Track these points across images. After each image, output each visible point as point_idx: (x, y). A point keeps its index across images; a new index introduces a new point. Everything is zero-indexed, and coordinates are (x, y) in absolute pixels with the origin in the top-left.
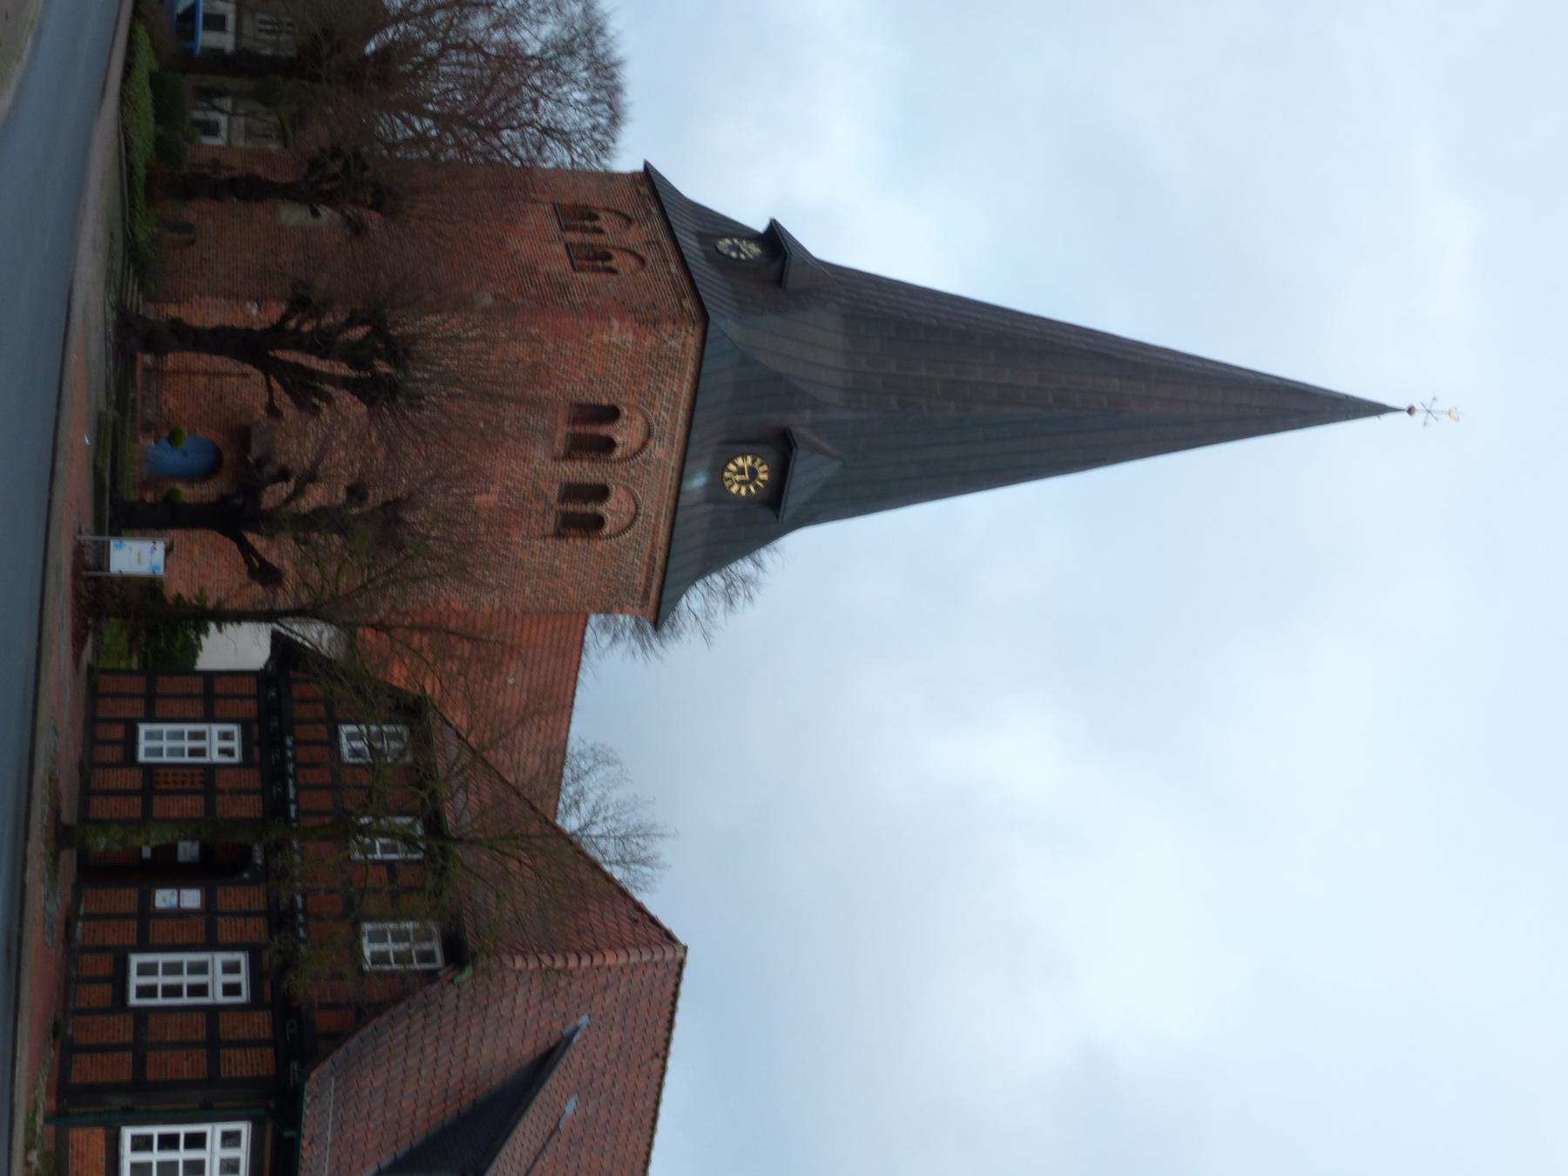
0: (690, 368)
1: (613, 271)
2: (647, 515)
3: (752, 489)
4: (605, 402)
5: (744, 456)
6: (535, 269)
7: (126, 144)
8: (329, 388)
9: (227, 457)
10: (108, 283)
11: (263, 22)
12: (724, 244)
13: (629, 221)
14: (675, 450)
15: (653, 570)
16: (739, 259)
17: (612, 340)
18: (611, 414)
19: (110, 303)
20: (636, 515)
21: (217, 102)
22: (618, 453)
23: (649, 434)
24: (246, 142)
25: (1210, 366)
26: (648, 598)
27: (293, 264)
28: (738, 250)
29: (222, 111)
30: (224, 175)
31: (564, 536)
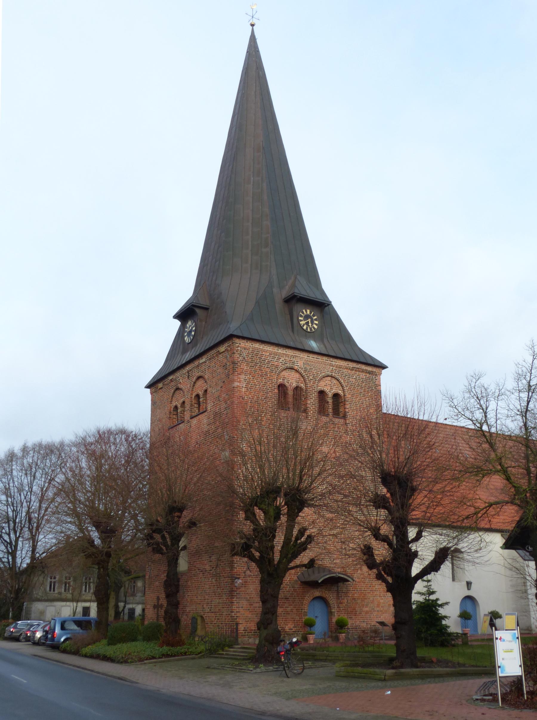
0: (257, 345)
1: (206, 391)
4: (276, 391)
5: (299, 321)
6: (206, 432)
7: (150, 659)
8: (295, 532)
9: (317, 593)
10: (241, 671)
11: (85, 591)
12: (187, 339)
13: (178, 389)
14: (299, 355)
15: (359, 368)
16: (195, 331)
17: (244, 386)
18: (282, 387)
19: (255, 668)
20: (331, 376)
21: (121, 609)
23: (292, 368)
24: (137, 596)
25: (237, 111)
26: (373, 372)
27: (211, 561)
28: (190, 332)
29: (124, 607)
30: (164, 602)
31: (345, 414)
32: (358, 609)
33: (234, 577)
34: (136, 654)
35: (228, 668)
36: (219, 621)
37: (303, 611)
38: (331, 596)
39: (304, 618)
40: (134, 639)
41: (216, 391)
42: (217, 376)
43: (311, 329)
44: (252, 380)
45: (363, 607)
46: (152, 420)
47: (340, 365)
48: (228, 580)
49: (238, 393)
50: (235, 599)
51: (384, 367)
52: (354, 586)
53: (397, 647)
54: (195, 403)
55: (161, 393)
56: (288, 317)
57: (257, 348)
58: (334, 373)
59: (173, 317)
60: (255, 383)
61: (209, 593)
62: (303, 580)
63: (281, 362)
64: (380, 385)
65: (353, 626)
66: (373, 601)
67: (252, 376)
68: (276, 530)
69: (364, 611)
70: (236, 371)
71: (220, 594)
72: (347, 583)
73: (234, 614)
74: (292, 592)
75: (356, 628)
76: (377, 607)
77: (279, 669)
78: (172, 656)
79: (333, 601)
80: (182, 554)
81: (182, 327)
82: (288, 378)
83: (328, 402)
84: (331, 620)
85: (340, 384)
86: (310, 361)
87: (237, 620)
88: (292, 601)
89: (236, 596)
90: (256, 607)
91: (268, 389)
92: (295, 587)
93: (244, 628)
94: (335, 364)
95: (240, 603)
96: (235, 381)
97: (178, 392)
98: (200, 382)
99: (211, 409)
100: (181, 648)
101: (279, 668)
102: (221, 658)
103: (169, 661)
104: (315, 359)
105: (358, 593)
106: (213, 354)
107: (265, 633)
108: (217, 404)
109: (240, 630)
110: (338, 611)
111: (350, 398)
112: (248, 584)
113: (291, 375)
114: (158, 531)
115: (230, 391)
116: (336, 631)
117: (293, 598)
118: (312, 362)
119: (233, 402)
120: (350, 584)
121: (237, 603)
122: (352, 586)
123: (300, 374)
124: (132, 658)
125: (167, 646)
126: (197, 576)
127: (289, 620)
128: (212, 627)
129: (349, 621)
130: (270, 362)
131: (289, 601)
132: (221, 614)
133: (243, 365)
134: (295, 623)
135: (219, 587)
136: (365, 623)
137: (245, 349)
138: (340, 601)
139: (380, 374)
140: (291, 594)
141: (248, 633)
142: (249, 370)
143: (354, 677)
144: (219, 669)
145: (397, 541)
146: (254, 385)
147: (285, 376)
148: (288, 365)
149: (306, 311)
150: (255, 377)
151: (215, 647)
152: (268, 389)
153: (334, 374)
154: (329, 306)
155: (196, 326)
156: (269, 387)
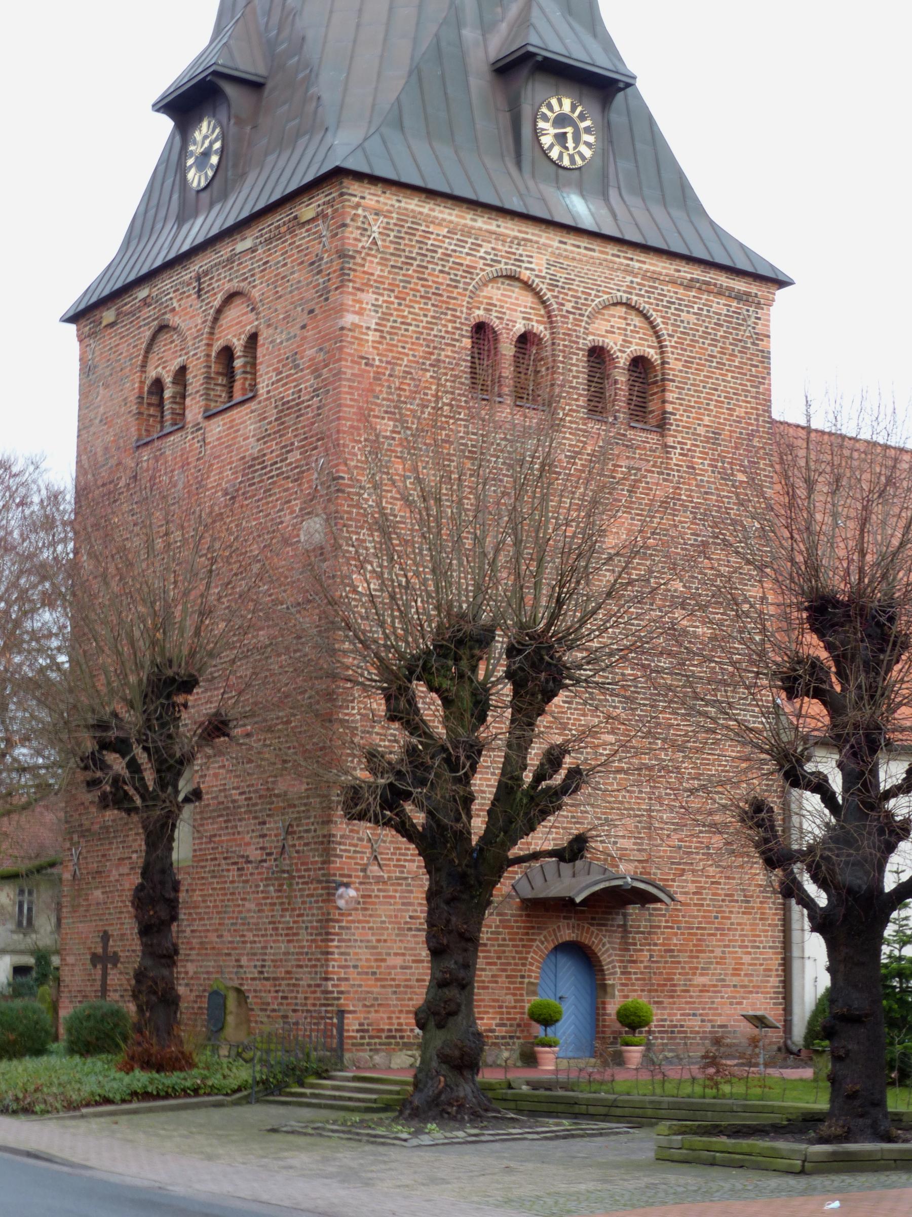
0: (412, 204)
1: (253, 338)
2: (630, 290)
3: (588, 123)
4: (467, 342)
5: (536, 134)
6: (254, 459)
7: (97, 1104)
8: (535, 755)
9: (567, 934)
10: (374, 1140)
12: (195, 178)
13: (163, 328)
14: (535, 238)
15: (707, 283)
16: (222, 152)
17: (373, 326)
20: (628, 305)
22: (539, 328)
23: (513, 278)
26: (748, 294)
27: (263, 836)
28: (206, 154)
31: (664, 418)
32: (679, 980)
33: (334, 881)
34: (54, 1089)
35: (333, 1131)
36: (288, 1004)
37: (526, 980)
38: (605, 940)
39: (529, 1001)
40: (39, 1051)
41: (288, 340)
42: (291, 292)
43: (572, 158)
44: (396, 310)
45: (694, 974)
46: (81, 419)
47: (654, 272)
48: (315, 889)
49: (355, 346)
50: (336, 943)
51: (781, 283)
52: (671, 916)
53: (833, 1084)
54: (218, 373)
55: (111, 339)
56: (505, 119)
57: (413, 211)
58: (637, 295)
59: (154, 106)
60: (403, 317)
61: (257, 924)
62: (529, 894)
63: (481, 258)
64: (769, 336)
65: (663, 1026)
66: (721, 958)
67: (396, 297)
68: (479, 753)
69: (698, 986)
70: (350, 281)
71: (291, 928)
72: (652, 906)
73: (333, 986)
74: (497, 927)
75: (672, 1032)
76: (733, 975)
77: (483, 1138)
78: (158, 1097)
79: (610, 956)
80: (187, 811)
81: (178, 138)
82: (502, 307)
83: (616, 382)
84: (604, 1009)
85: (654, 327)
86: (567, 257)
87: (342, 1001)
88: (495, 951)
89: (337, 934)
90: (395, 967)
91: (444, 338)
92: (506, 914)
93: (361, 1024)
94: (640, 268)
95: (349, 954)
96: (348, 311)
97: (164, 337)
98: (234, 312)
99: (268, 392)
100: (182, 1075)
101: (483, 1135)
102: (300, 1105)
103: (150, 1110)
104: (582, 251)
105: (682, 934)
106: (279, 227)
107: (439, 1039)
108: (287, 377)
109: (348, 1031)
110: (623, 985)
111: (681, 371)
112: (374, 903)
113: (510, 297)
114: (121, 747)
115: (330, 339)
116: (615, 1038)
117: (499, 945)
118: (574, 259)
119: (340, 372)
120: (660, 909)
121: (341, 954)
122: (664, 915)
123: (537, 294)
124: (45, 1102)
125: (142, 1068)
126: (221, 877)
127: (485, 1006)
128: (265, 1020)
129: (654, 1012)
130: (450, 256)
131: (489, 951)
132: (294, 985)
133: (372, 262)
134: (502, 1013)
135: (287, 910)
136: (699, 1018)
137: (376, 214)
138: (631, 956)
139: (770, 303)
140: (492, 933)
141: (370, 1037)
142: (388, 278)
143: (713, 1163)
144: (305, 1134)
145: (846, 789)
146: (402, 323)
147: (491, 298)
148: (502, 266)
149: (561, 104)
150: (405, 299)
151: (280, 1076)
152: (444, 338)
153: (635, 298)
154: (629, 90)
155: (224, 137)
156: (447, 332)
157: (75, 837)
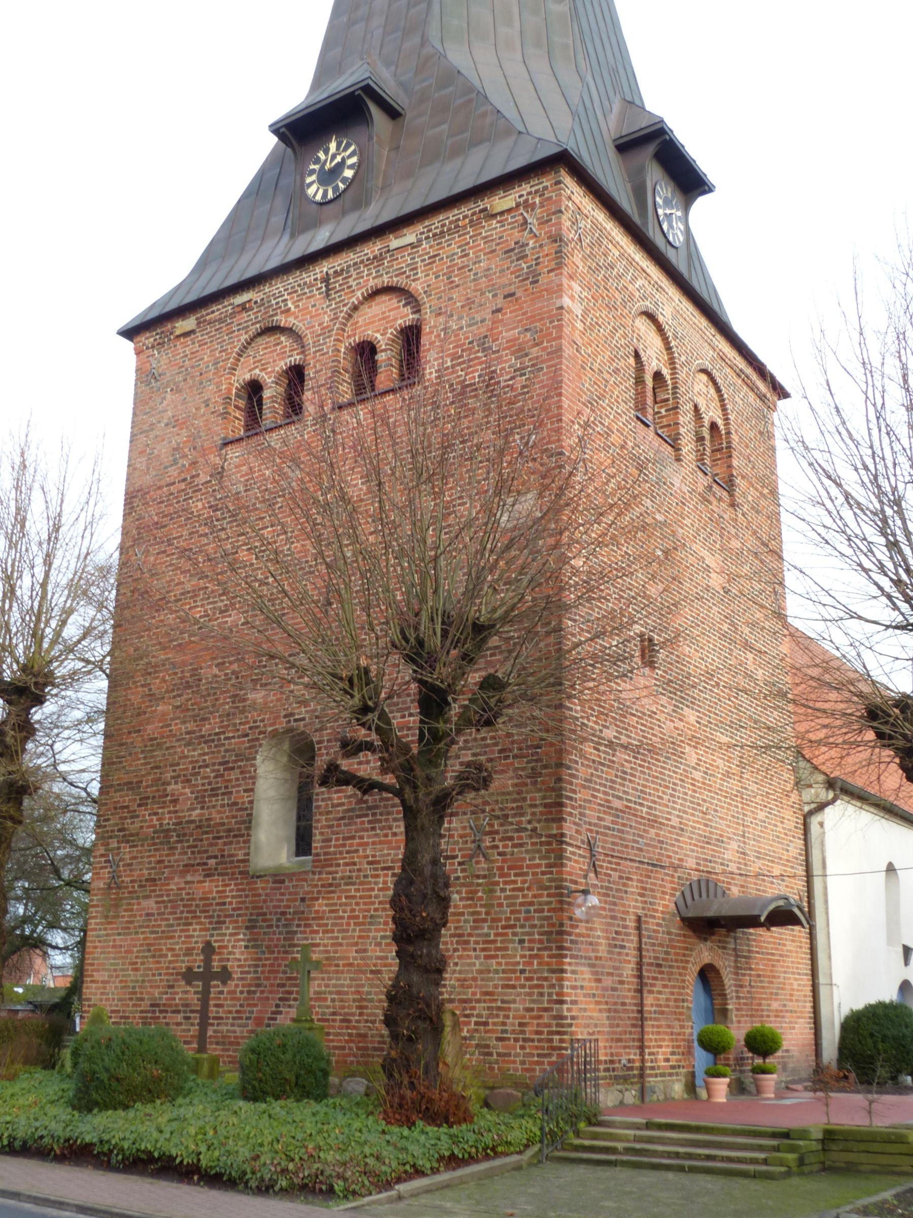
54: (346, 371)
59: (270, 126)
87: (573, 1029)
157: (114, 844)
